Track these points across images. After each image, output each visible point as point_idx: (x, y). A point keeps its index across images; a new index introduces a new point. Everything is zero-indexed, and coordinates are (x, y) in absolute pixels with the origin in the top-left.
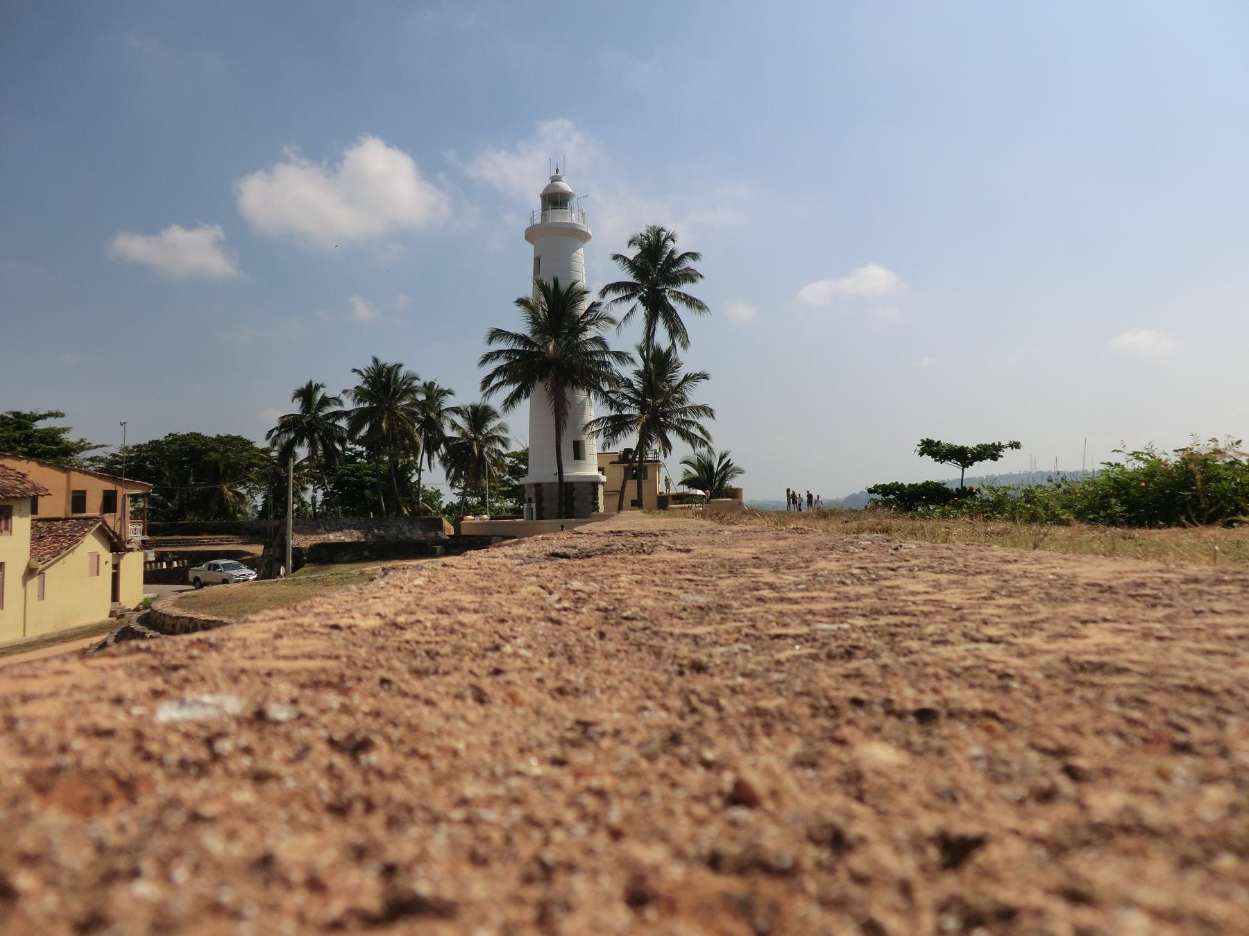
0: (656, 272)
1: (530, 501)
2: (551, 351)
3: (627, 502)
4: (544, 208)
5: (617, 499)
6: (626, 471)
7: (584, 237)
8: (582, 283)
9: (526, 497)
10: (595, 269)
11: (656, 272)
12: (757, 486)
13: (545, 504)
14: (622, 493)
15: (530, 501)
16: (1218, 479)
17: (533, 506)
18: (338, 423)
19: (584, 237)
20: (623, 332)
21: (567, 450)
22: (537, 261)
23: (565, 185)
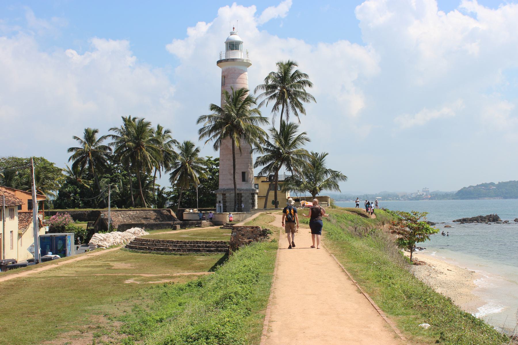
0: (287, 86)
1: (220, 202)
2: (230, 120)
3: (269, 204)
4: (227, 50)
5: (264, 200)
6: (270, 185)
7: (248, 65)
8: (247, 87)
9: (218, 200)
10: (253, 81)
11: (287, 86)
12: (312, 245)
13: (227, 204)
14: (266, 197)
16: (424, 315)
17: (222, 205)
18: (149, 192)
19: (248, 65)
20: (269, 118)
21: (239, 177)
22: (224, 77)
23: (236, 38)
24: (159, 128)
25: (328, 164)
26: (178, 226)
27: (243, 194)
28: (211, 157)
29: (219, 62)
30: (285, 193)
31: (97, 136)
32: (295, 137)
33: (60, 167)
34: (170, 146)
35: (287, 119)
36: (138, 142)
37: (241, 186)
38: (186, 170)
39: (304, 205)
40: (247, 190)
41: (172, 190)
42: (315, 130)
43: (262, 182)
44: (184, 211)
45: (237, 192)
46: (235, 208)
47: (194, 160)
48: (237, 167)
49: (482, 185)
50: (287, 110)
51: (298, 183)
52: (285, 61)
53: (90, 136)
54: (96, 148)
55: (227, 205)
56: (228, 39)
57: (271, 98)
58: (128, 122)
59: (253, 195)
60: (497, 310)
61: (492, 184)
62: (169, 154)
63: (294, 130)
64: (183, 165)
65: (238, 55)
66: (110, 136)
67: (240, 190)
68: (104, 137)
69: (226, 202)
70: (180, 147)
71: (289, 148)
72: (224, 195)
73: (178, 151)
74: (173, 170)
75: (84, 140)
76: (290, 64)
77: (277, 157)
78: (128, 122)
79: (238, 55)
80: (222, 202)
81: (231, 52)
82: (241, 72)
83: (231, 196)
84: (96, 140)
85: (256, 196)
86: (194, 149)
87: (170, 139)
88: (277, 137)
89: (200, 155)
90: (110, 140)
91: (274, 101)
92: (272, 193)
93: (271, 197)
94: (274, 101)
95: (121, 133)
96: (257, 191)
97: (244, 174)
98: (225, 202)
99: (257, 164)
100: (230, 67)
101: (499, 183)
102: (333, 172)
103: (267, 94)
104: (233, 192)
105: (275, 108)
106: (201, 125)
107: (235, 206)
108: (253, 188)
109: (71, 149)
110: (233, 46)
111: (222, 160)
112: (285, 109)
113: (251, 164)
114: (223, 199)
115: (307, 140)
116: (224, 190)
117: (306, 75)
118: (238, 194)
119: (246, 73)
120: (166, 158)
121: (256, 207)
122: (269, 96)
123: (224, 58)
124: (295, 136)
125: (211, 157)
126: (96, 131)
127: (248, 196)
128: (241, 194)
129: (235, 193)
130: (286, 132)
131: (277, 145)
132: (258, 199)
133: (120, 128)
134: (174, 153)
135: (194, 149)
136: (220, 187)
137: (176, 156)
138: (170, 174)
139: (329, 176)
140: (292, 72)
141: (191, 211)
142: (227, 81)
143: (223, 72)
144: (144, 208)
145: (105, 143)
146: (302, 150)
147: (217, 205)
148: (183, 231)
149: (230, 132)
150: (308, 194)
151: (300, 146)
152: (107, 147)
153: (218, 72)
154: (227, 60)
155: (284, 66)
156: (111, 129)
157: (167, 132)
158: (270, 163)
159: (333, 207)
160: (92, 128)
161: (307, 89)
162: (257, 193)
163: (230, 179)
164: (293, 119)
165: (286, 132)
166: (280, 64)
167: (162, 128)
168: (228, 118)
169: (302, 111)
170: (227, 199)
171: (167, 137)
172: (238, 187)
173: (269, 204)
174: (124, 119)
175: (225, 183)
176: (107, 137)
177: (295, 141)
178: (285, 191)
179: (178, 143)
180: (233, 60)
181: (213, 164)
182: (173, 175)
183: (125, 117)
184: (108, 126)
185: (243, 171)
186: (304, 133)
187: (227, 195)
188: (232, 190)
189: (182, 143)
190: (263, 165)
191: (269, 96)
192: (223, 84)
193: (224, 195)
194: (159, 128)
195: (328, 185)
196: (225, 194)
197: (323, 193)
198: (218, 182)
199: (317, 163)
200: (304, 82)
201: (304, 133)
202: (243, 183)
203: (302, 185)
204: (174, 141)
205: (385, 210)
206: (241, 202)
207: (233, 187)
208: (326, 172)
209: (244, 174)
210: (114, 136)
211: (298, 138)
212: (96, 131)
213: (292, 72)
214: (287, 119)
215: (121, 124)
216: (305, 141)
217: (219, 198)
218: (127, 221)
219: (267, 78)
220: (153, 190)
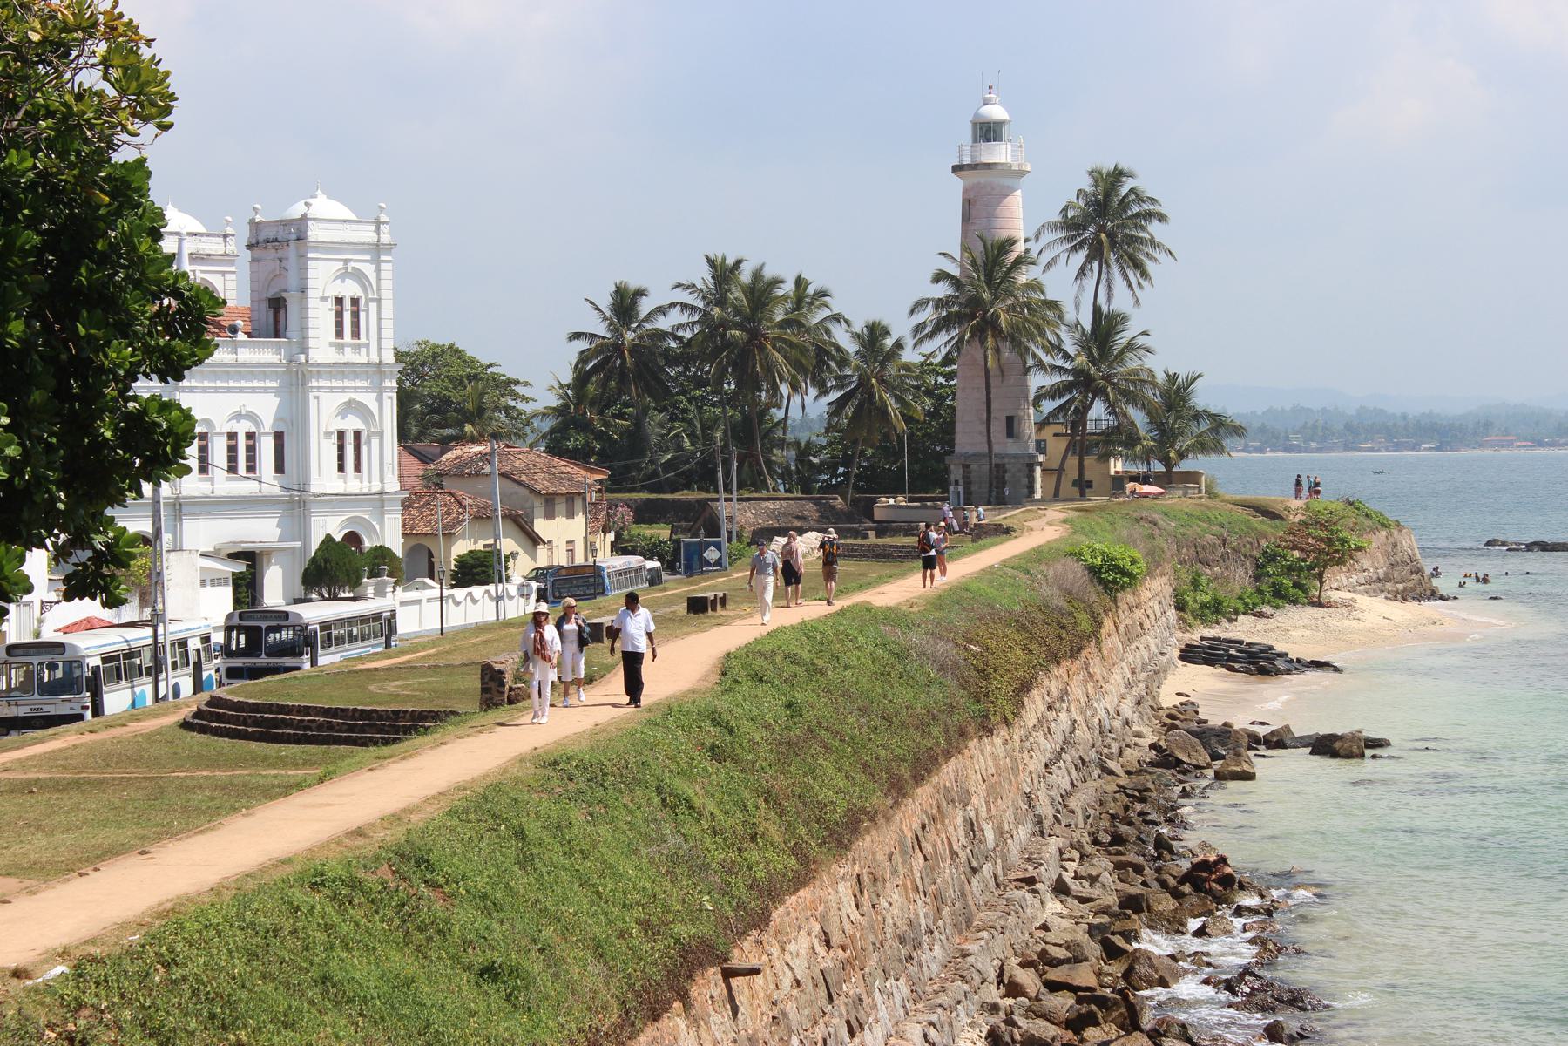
0: (1110, 222)
1: (957, 483)
2: (984, 294)
3: (1067, 487)
4: (975, 141)
5: (1054, 478)
9: (953, 478)
11: (1110, 222)
13: (974, 488)
14: (1061, 470)
15: (957, 483)
17: (961, 489)
21: (998, 428)
22: (968, 204)
23: (996, 112)
24: (800, 283)
25: (1203, 398)
26: (872, 534)
29: (957, 169)
30: (1108, 461)
31: (645, 306)
32: (1123, 342)
33: (512, 375)
34: (828, 332)
35: (1109, 300)
36: (750, 326)
37: (1004, 446)
38: (872, 395)
39: (1133, 492)
40: (1015, 456)
41: (824, 441)
42: (1177, 324)
44: (875, 501)
45: (995, 460)
47: (892, 370)
50: (1109, 282)
51: (1132, 440)
52: (1107, 166)
53: (625, 304)
54: (641, 338)
56: (976, 115)
57: (1074, 249)
58: (723, 273)
59: (1030, 468)
62: (828, 353)
63: (1120, 327)
64: (863, 383)
65: (1000, 153)
66: (673, 305)
67: (1002, 456)
68: (662, 310)
70: (857, 336)
71: (1110, 366)
72: (966, 467)
73: (851, 347)
74: (835, 395)
75: (608, 313)
76: (1118, 175)
77: (1084, 384)
78: (723, 273)
79: (1000, 153)
81: (984, 145)
82: (1006, 192)
83: (980, 470)
84: (643, 314)
85: (1038, 470)
86: (889, 342)
88: (1085, 343)
90: (675, 318)
91: (1081, 256)
92: (1073, 461)
93: (1072, 473)
94: (1081, 256)
95: (704, 298)
96: (1041, 458)
97: (1010, 421)
98: (968, 484)
100: (982, 180)
102: (1214, 417)
103: (1063, 241)
104: (985, 461)
105: (1082, 273)
106: (920, 317)
108: (1032, 451)
109: (577, 336)
110: (988, 131)
111: (963, 389)
112: (1104, 277)
113: (1027, 397)
115: (1148, 350)
116: (967, 456)
117: (1153, 201)
119: (1019, 192)
120: (817, 361)
121: (1038, 495)
122: (1068, 246)
123: (967, 160)
124: (1122, 340)
126: (641, 293)
130: (1104, 328)
131: (1082, 360)
132: (1043, 475)
133: (700, 285)
134: (839, 349)
135: (889, 342)
136: (958, 449)
137: (843, 361)
139: (1205, 426)
140: (1124, 190)
141: (891, 501)
142: (974, 212)
143: (965, 191)
144: (765, 493)
145: (664, 323)
146: (1136, 372)
147: (951, 488)
148: (880, 541)
149: (979, 333)
150: (1158, 467)
151: (1132, 363)
152: (666, 333)
153: (956, 186)
154: (974, 167)
155: (1105, 180)
156: (679, 285)
157: (823, 294)
158: (1068, 397)
159: (1211, 494)
160: (633, 284)
161: (1154, 228)
162: (1040, 464)
164: (1121, 301)
165: (1104, 328)
166: (1095, 174)
167: (807, 284)
168: (975, 303)
169: (1144, 274)
171: (818, 307)
172: (996, 449)
173: (1067, 487)
174: (711, 263)
175: (968, 439)
176: (671, 310)
177: (1122, 351)
178: (1105, 458)
179: (847, 323)
180: (989, 166)
181: (938, 374)
182: (839, 406)
183: (712, 257)
184: (671, 288)
186: (1145, 333)
187: (974, 467)
189: (858, 326)
191: (1068, 246)
192: (966, 218)
193: (966, 467)
194: (800, 283)
195: (1202, 447)
197: (1186, 465)
198: (953, 423)
199: (1176, 395)
200: (1149, 215)
201: (1145, 333)
203: (1138, 448)
204: (837, 318)
205: (1351, 504)
206: (1004, 483)
208: (1197, 416)
209: (1010, 421)
210: (684, 306)
211: (1130, 346)
212: (641, 293)
213: (1124, 190)
214: (1109, 300)
215: (702, 276)
216: (1142, 352)
217: (956, 473)
218: (763, 522)
219: (1065, 210)
220: (782, 444)
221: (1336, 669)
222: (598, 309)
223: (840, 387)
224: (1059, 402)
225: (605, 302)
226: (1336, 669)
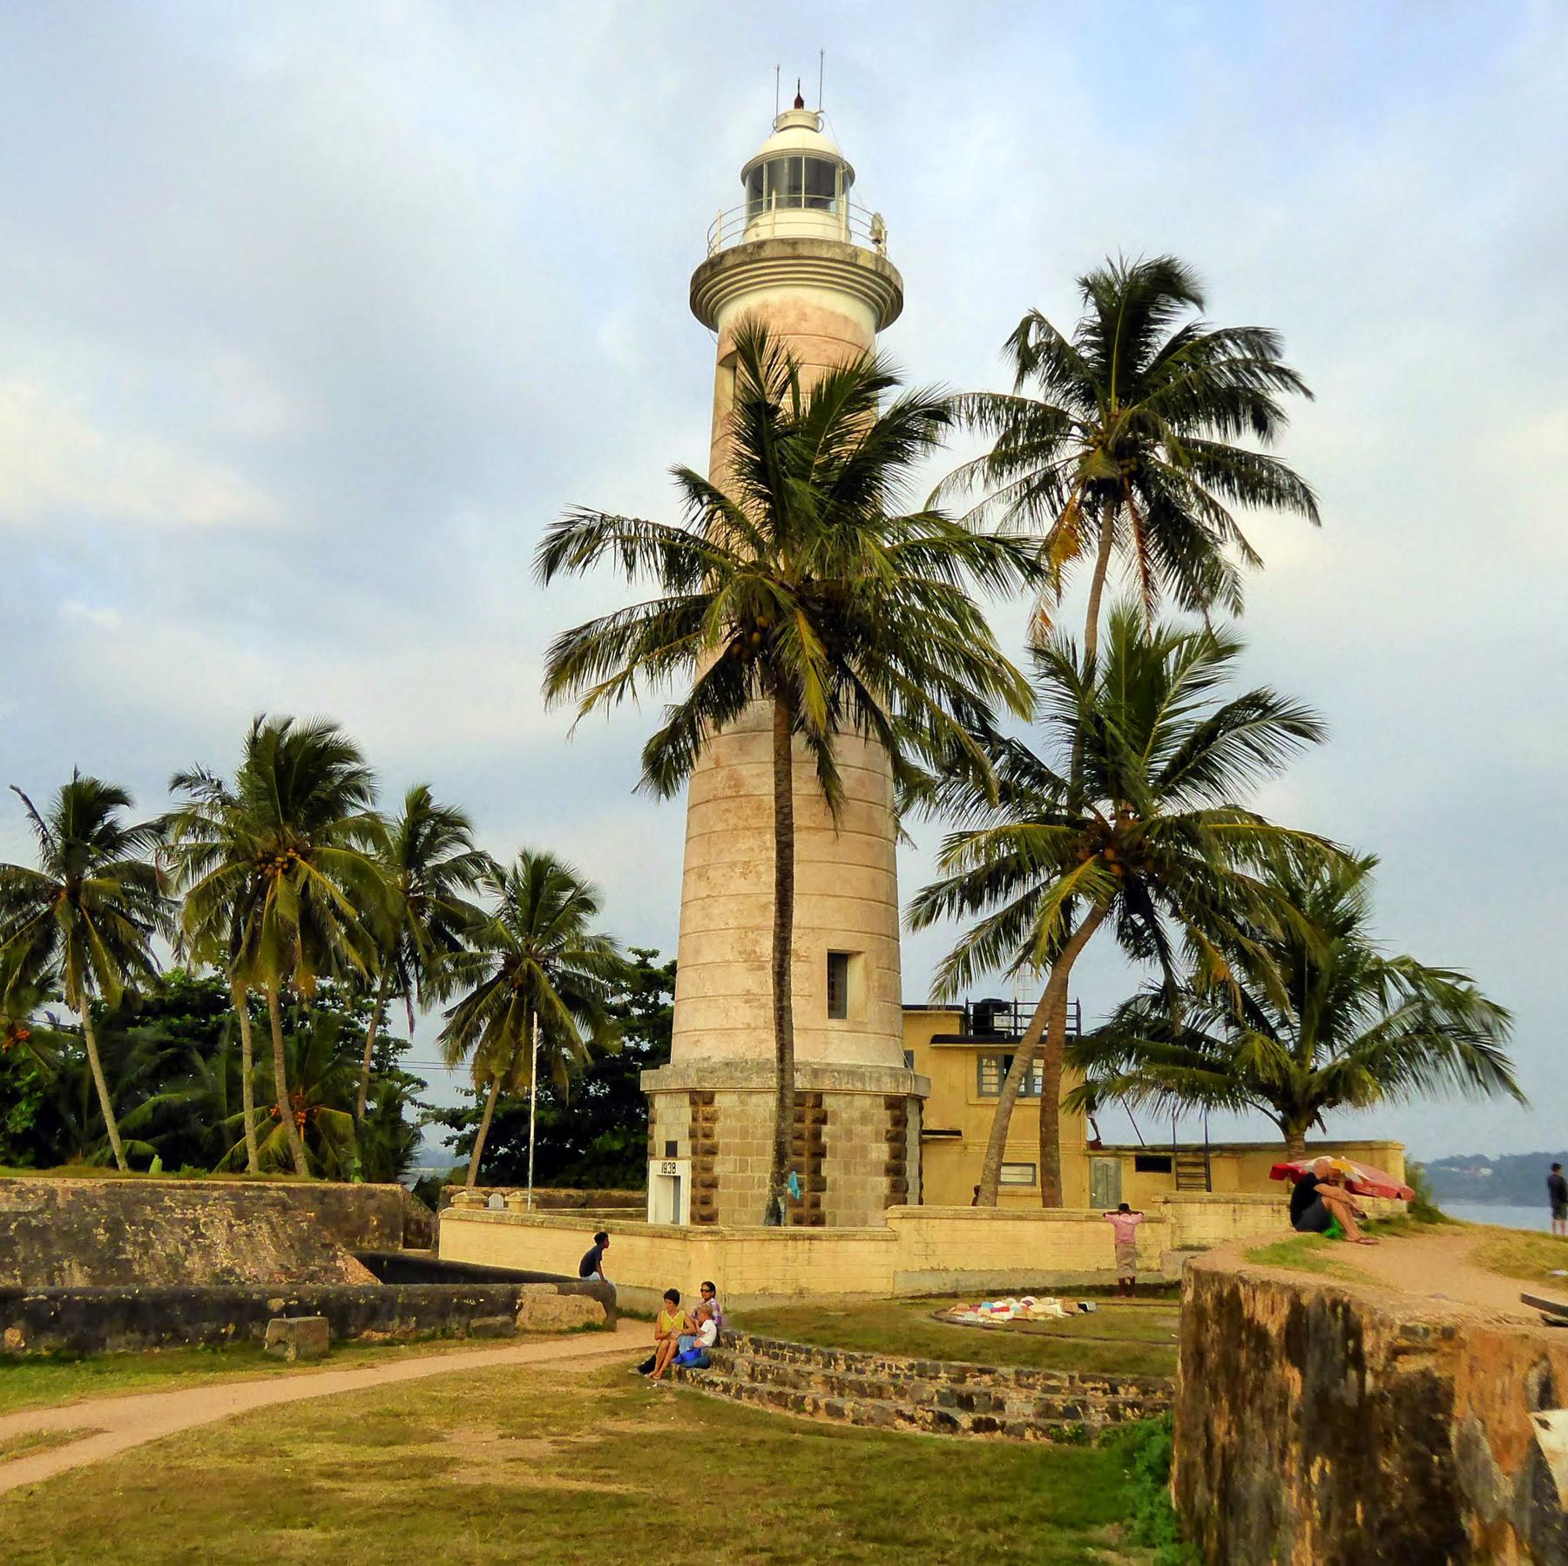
0: (1154, 401)
1: (672, 1149)
9: (660, 1135)
11: (1154, 401)
13: (722, 1167)
17: (684, 1168)
21: (808, 980)
25: (1389, 927)
27: (829, 1103)
28: (654, 954)
43: (936, 1039)
46: (777, 1193)
48: (798, 915)
49: (1451, 1162)
53: (86, 809)
55: (718, 1170)
60: (1359, 1507)
61: (1480, 1160)
69: (712, 1151)
72: (701, 1099)
74: (460, 994)
76: (1165, 282)
80: (684, 1148)
87: (466, 850)
89: (593, 926)
99: (929, 906)
101: (1503, 1157)
102: (1417, 974)
107: (780, 1179)
114: (693, 1135)
118: (801, 1097)
125: (654, 954)
127: (865, 1119)
128: (819, 1097)
129: (783, 1089)
132: (1170, 1500)
136: (680, 1049)
138: (449, 1014)
147: (655, 1167)
158: (1018, 892)
163: (749, 998)
170: (723, 1132)
172: (802, 1052)
185: (838, 945)
188: (761, 1067)
190: (976, 903)
193: (701, 1099)
196: (709, 1099)
202: (835, 1023)
207: (770, 1050)
212: (118, 797)
217: (670, 1120)
221: (1308, 393)
222: (34, 815)
223: (469, 980)
224: (992, 909)
225: (50, 805)
226: (1308, 393)
